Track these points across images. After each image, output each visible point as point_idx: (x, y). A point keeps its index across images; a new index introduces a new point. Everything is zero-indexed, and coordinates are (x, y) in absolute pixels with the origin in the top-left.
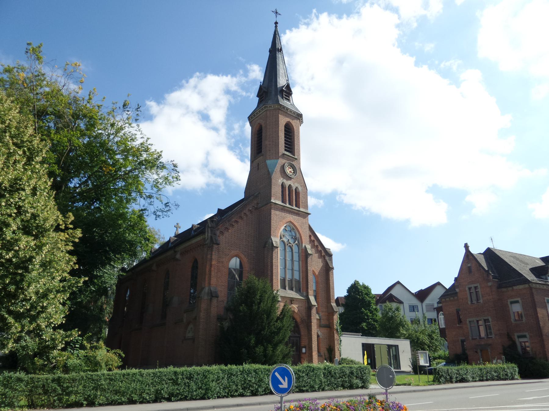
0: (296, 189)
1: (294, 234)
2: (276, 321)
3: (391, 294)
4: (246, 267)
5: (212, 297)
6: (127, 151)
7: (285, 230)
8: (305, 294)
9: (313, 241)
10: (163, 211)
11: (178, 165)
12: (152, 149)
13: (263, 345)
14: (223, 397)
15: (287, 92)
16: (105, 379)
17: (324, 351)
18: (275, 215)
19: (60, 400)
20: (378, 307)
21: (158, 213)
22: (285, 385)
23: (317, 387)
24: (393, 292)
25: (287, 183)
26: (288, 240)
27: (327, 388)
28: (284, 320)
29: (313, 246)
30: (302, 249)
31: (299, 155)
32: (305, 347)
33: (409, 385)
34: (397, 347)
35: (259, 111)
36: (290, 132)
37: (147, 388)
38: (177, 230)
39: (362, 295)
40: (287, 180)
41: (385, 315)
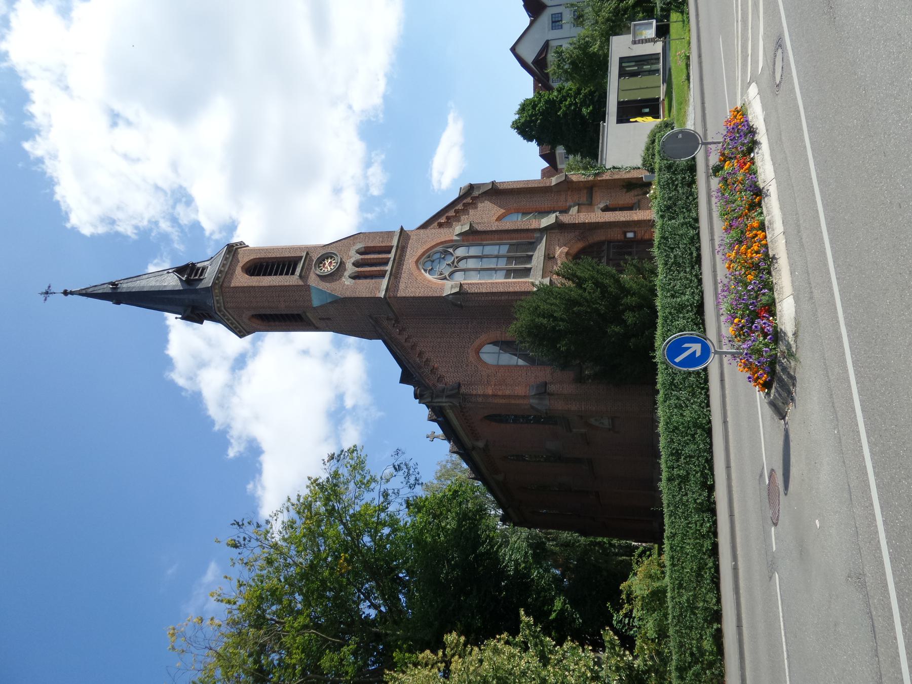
1: (438, 256)
2: (585, 290)
3: (534, 63)
4: (496, 334)
5: (545, 392)
6: (311, 534)
7: (431, 271)
8: (537, 235)
9: (448, 218)
10: (408, 475)
11: (331, 452)
12: (305, 492)
13: (624, 311)
14: (708, 397)
15: (189, 272)
16: (680, 595)
17: (628, 198)
18: (406, 289)
19: (711, 665)
20: (556, 85)
21: (412, 481)
22: (697, 348)
23: (692, 232)
24: (530, 59)
25: (350, 269)
26: (448, 265)
27: (694, 215)
28: (582, 275)
29: (457, 218)
30: (463, 241)
31: (300, 248)
32: (625, 233)
33: (688, 58)
34: (622, 60)
35: (228, 320)
36: (261, 266)
37: (693, 526)
39: (535, 115)
40: (345, 270)
41: (569, 76)
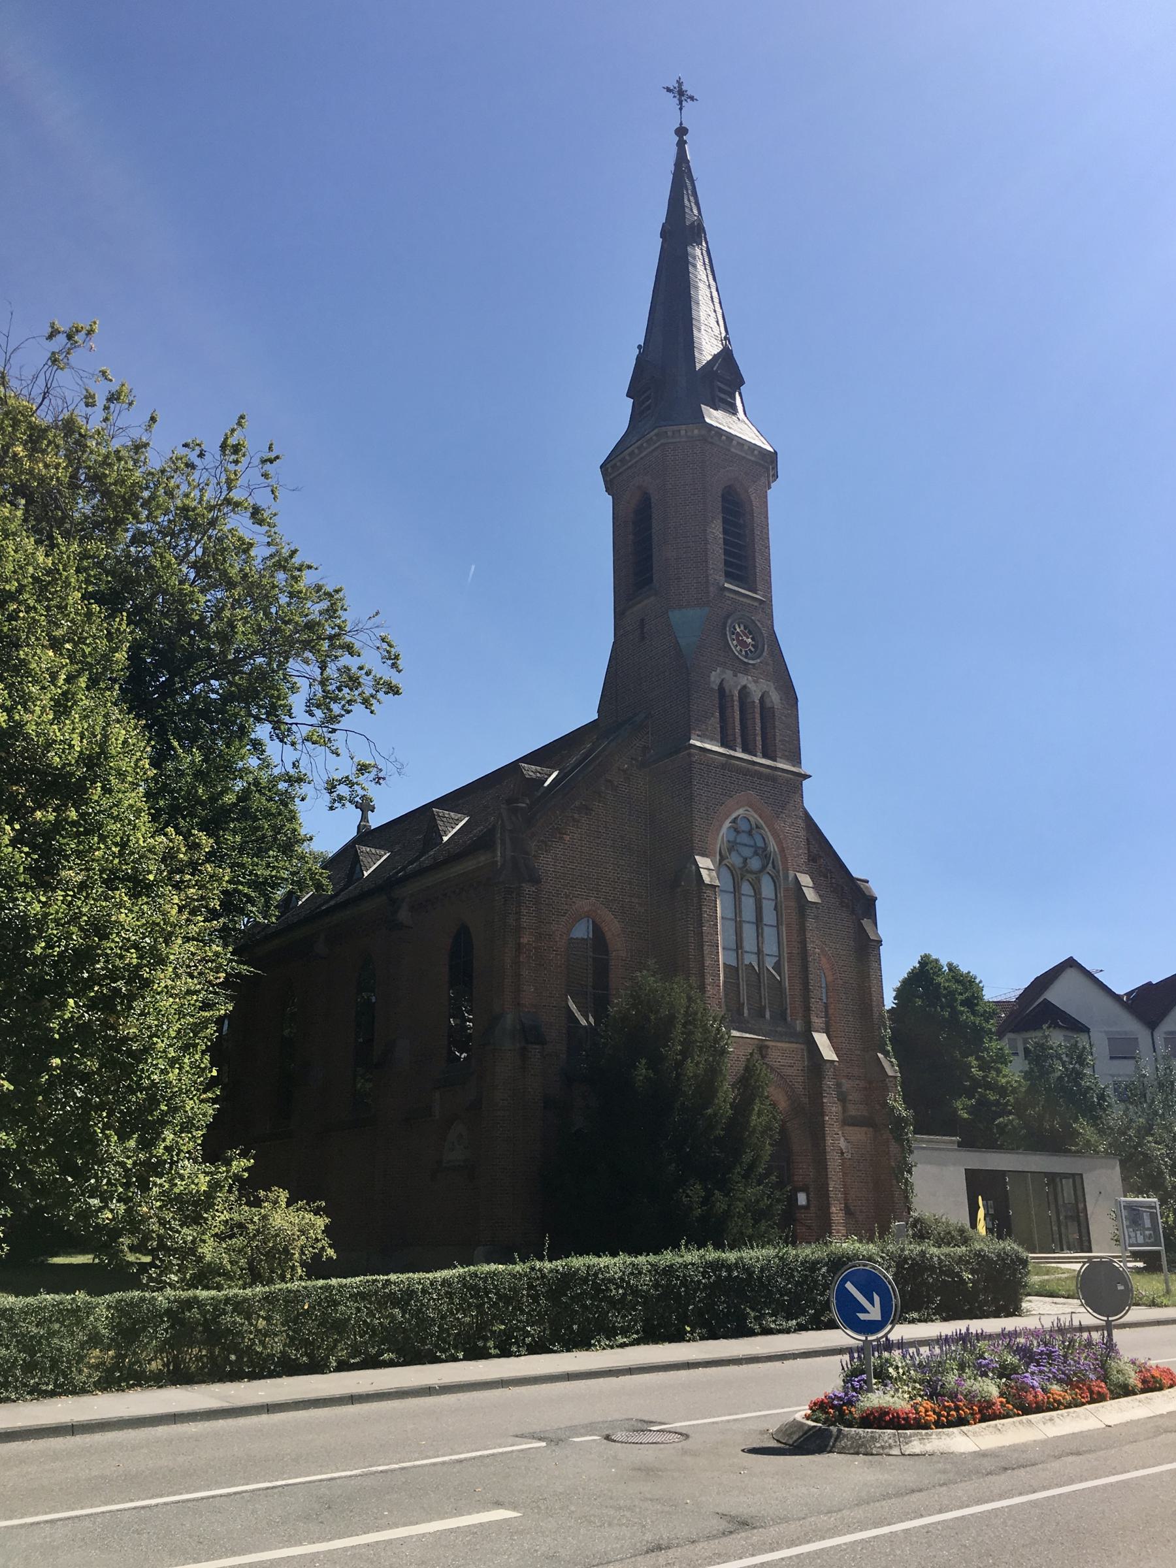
0: (762, 699)
22: (874, 1313)
24: (1054, 995)
32: (805, 1189)
38: (364, 818)
